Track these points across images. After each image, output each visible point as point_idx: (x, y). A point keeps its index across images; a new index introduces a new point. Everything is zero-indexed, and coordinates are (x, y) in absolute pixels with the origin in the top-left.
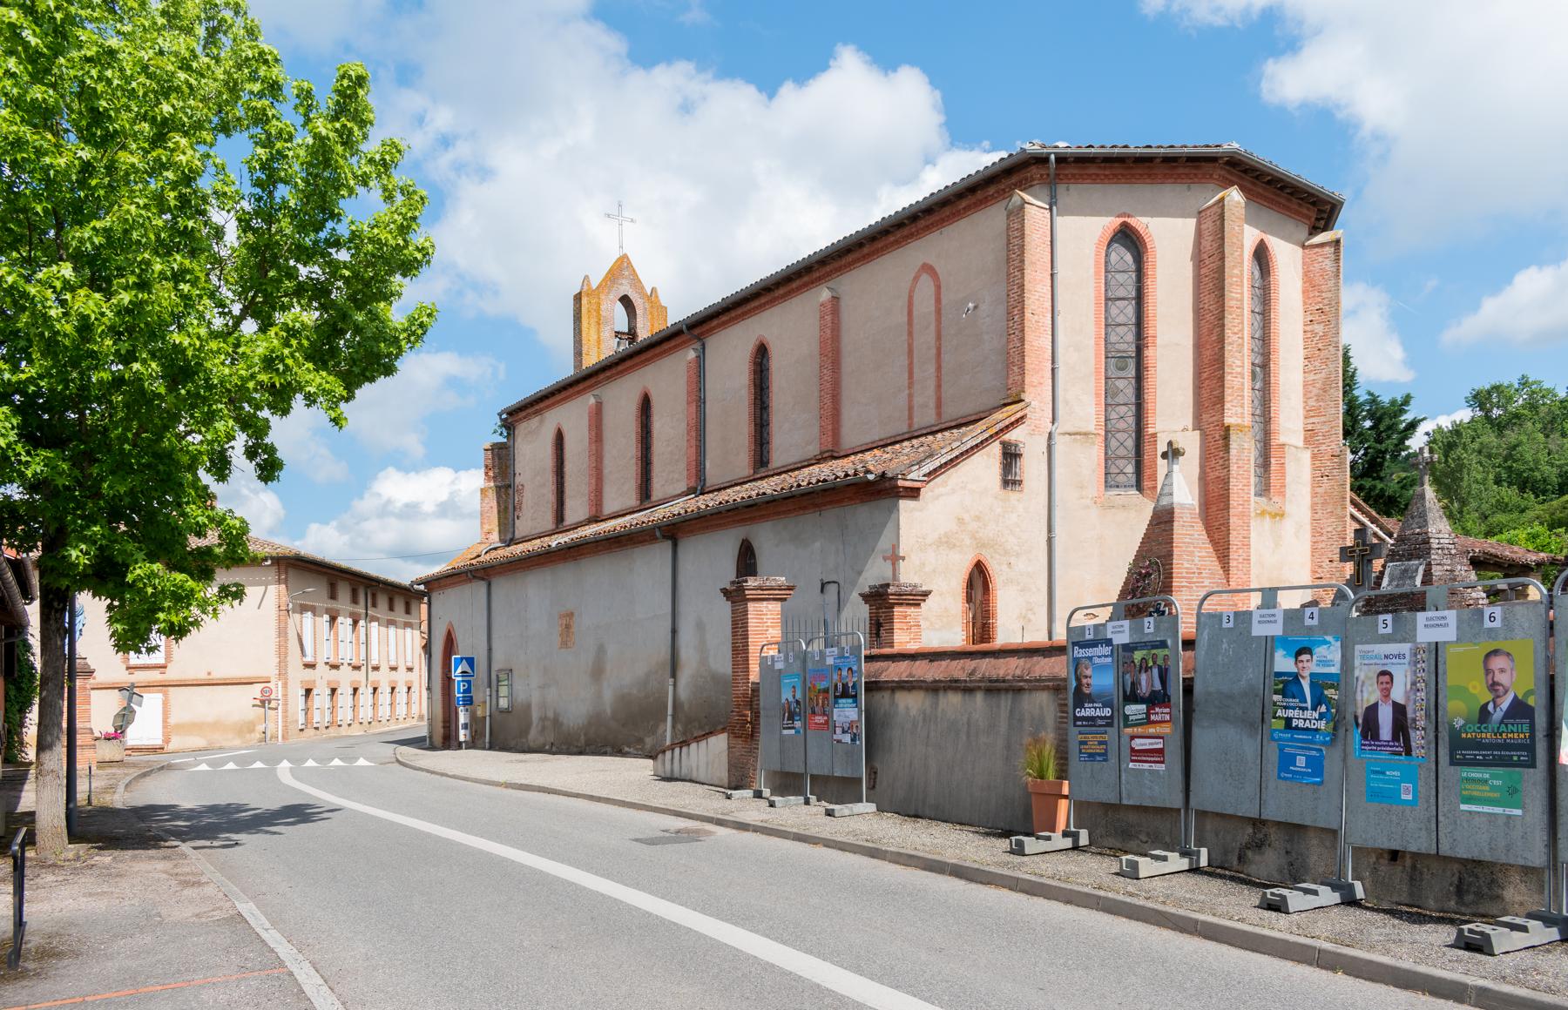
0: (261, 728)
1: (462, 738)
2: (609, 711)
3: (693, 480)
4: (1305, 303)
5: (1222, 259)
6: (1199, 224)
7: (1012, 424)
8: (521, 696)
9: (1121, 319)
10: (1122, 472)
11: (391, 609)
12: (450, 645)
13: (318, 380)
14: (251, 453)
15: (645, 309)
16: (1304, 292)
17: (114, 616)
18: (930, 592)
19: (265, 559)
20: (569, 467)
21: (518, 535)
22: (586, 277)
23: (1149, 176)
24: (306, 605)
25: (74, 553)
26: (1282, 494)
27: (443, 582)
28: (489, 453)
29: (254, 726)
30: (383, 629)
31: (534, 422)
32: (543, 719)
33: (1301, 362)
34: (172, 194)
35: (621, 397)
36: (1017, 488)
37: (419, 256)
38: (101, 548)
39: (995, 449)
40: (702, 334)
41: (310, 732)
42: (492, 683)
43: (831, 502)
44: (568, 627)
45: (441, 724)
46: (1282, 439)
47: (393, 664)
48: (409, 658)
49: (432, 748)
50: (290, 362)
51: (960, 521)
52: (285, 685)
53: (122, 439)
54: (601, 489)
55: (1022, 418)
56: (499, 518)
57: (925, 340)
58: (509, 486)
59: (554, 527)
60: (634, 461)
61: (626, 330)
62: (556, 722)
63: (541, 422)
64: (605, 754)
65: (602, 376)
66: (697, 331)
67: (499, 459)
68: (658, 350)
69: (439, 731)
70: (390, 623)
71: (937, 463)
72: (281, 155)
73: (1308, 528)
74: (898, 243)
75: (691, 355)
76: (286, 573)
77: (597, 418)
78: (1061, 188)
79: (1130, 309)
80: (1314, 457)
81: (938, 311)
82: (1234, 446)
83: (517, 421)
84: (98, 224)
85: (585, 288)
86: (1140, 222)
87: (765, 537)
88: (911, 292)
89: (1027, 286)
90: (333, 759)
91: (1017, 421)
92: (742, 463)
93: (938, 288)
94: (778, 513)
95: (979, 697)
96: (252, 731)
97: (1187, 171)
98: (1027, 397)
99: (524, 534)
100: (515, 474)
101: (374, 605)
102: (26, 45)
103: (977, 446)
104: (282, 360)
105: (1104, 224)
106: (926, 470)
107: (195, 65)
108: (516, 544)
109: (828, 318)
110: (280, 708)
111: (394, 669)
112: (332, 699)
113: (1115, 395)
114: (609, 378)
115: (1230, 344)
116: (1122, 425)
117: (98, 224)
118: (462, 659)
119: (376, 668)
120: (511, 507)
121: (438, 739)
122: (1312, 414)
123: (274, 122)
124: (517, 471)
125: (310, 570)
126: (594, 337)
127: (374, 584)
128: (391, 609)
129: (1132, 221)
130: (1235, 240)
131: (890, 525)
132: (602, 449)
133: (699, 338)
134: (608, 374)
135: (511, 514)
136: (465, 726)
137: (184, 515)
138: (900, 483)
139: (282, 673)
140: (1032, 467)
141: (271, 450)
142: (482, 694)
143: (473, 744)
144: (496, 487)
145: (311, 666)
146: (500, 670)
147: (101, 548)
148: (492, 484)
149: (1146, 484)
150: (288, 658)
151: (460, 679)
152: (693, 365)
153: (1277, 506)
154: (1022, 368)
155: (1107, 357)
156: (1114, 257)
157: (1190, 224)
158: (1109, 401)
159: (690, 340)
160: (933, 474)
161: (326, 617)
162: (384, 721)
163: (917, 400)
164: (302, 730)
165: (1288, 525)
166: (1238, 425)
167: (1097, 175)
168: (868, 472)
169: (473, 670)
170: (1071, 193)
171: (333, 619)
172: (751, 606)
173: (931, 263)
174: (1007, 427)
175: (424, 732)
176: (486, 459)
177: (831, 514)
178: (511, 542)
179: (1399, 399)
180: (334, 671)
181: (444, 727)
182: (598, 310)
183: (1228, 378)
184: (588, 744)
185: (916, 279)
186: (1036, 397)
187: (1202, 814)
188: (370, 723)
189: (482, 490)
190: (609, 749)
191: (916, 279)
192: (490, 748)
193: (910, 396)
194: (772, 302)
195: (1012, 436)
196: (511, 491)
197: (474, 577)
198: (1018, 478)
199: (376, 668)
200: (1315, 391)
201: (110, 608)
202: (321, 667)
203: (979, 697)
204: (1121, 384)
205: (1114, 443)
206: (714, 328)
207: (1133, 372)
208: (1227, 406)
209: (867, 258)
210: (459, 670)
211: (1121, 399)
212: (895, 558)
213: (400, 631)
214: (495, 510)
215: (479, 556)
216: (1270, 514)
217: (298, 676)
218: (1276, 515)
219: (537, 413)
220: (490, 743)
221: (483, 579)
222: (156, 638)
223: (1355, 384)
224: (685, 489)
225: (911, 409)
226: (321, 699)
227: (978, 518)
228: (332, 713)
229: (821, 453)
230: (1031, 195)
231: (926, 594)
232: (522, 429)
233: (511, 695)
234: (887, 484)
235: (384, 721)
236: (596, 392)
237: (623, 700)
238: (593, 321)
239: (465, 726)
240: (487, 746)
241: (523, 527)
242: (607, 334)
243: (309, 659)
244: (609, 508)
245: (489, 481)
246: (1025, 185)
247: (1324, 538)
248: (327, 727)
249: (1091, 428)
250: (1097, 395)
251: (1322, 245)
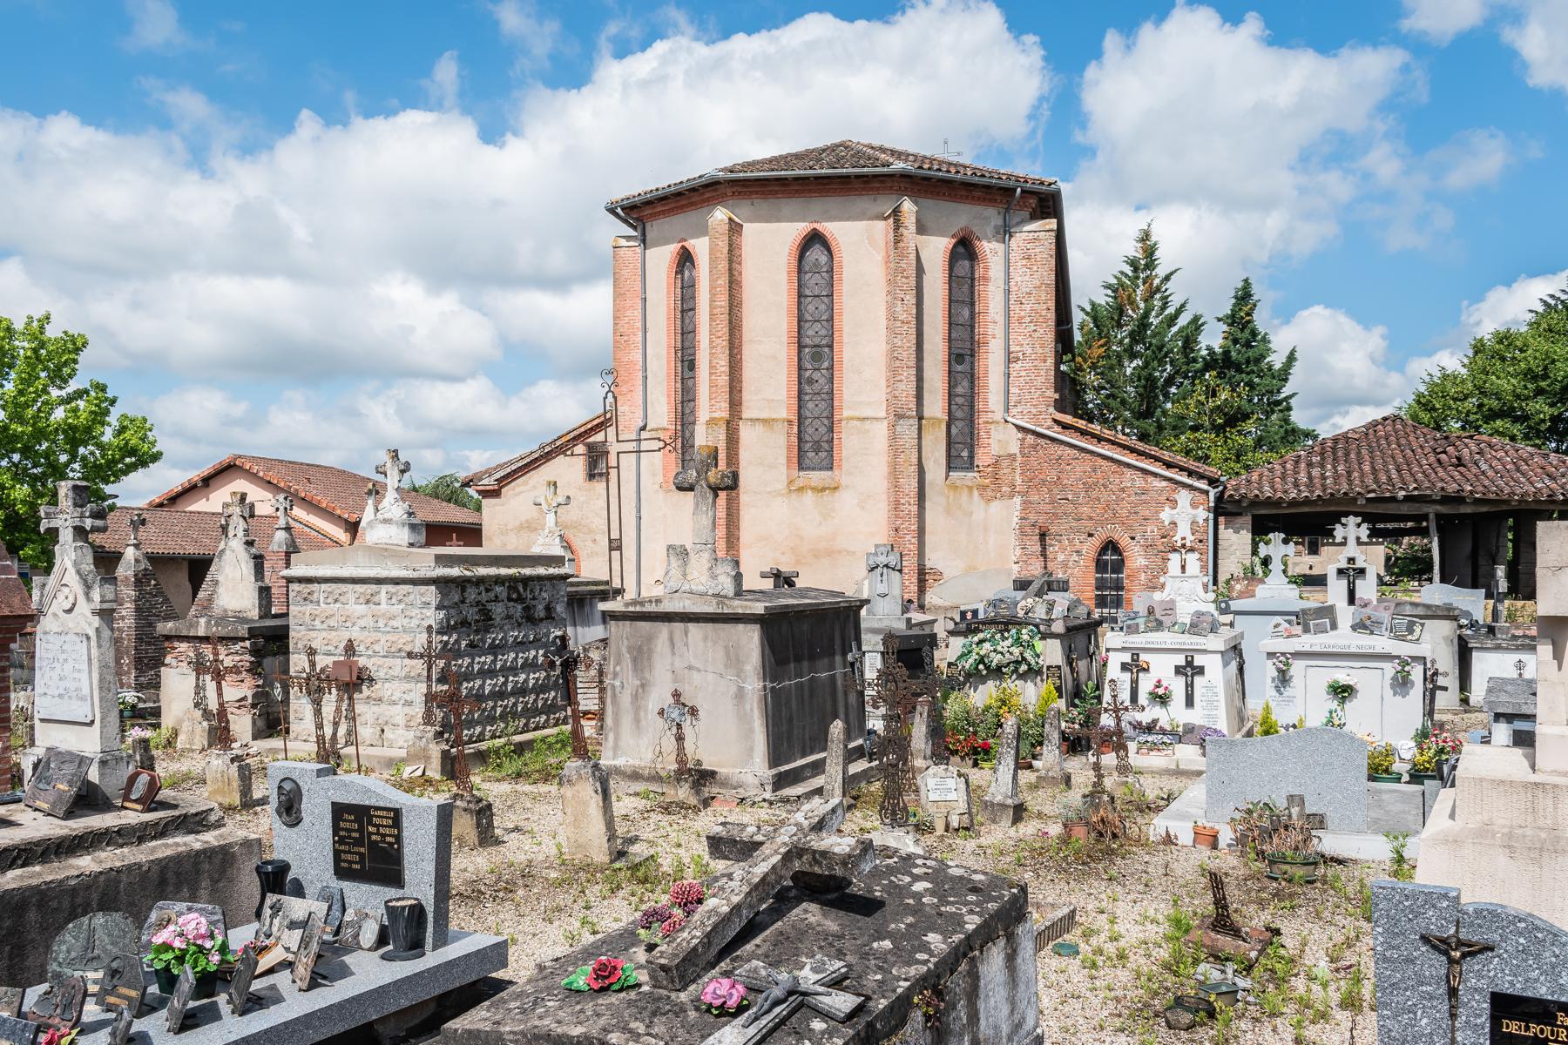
165: (846, 501)
216: (812, 489)
218: (823, 489)
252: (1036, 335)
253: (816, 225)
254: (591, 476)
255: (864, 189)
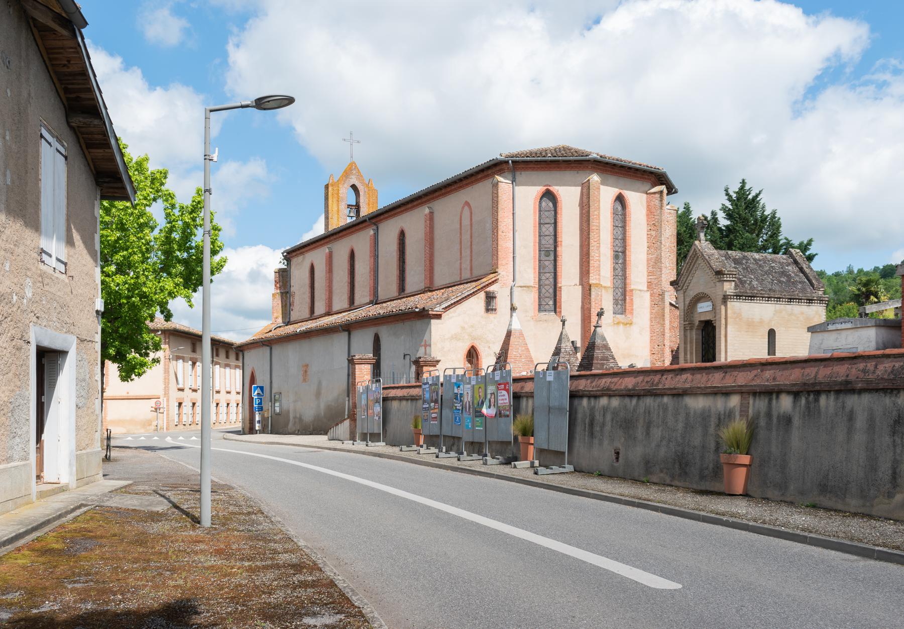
0: (155, 423)
1: (257, 428)
2: (323, 414)
3: (372, 297)
4: (647, 221)
5: (589, 207)
6: (582, 189)
7: (490, 283)
8: (285, 407)
9: (547, 233)
10: (547, 304)
11: (227, 357)
12: (253, 380)
13: (185, 292)
14: (162, 312)
15: (365, 192)
16: (647, 215)
17: (121, 370)
18: (440, 361)
19: (158, 331)
20: (316, 285)
21: (292, 319)
22: (331, 175)
23: (558, 168)
24: (179, 356)
25: (111, 351)
26: (632, 313)
27: (249, 346)
28: (277, 274)
29: (151, 422)
30: (222, 369)
31: (300, 258)
32: (295, 418)
33: (646, 249)
34: (144, 247)
35: (341, 248)
36: (494, 312)
37: (218, 249)
38: (118, 349)
39: (482, 295)
40: (377, 222)
41: (181, 427)
42: (273, 400)
43: (406, 319)
44: (306, 372)
45: (248, 422)
46: (632, 287)
47: (228, 390)
48: (228, 385)
49: (244, 434)
50: (176, 293)
51: (463, 328)
52: (168, 400)
53: (126, 316)
54: (332, 298)
55: (496, 280)
56: (282, 310)
57: (466, 237)
58: (288, 292)
59: (309, 316)
60: (346, 284)
61: (355, 204)
62: (301, 419)
63: (304, 259)
64: (321, 434)
65: (332, 238)
66: (374, 221)
67: (283, 277)
68: (357, 228)
69: (248, 425)
70: (227, 365)
71: (449, 303)
72: (174, 226)
73: (648, 329)
74: (456, 190)
75: (372, 232)
76: (169, 338)
77: (330, 258)
78: (518, 173)
79: (551, 229)
80: (651, 295)
81: (471, 225)
82: (593, 293)
83: (292, 257)
84: (122, 254)
85: (331, 181)
86: (555, 189)
87: (385, 332)
88: (461, 213)
89: (500, 219)
90: (192, 437)
91: (493, 282)
92: (394, 290)
93: (471, 213)
94: (388, 322)
95: (409, 401)
96: (150, 425)
97: (575, 165)
98: (499, 270)
99: (295, 319)
100: (290, 286)
101: (217, 355)
102: (104, 206)
103: (471, 294)
104: (174, 293)
105: (538, 190)
106: (444, 306)
107: (148, 198)
108: (291, 324)
109: (428, 222)
110: (165, 413)
111: (228, 392)
112: (193, 409)
113: (544, 268)
114: (335, 239)
115: (592, 246)
116: (547, 282)
117: (122, 254)
118: (257, 387)
119: (218, 392)
120: (288, 304)
121: (247, 430)
122: (650, 274)
123: (173, 217)
124: (292, 285)
125: (181, 336)
126: (335, 209)
127: (218, 343)
128: (227, 357)
129: (550, 188)
130: (595, 199)
131: (428, 330)
132: (332, 276)
133: (375, 224)
134: (335, 237)
135: (288, 308)
136: (259, 422)
137: (142, 337)
138: (430, 312)
139: (166, 394)
140: (502, 303)
141: (169, 311)
142: (267, 405)
143: (263, 431)
144: (281, 293)
145: (181, 390)
146: (275, 393)
147: (118, 349)
148: (279, 291)
149: (558, 310)
150: (170, 385)
151: (256, 397)
152: (372, 237)
153: (629, 319)
154: (497, 257)
155: (540, 251)
156: (544, 204)
157: (580, 188)
158: (542, 271)
159: (369, 225)
160: (447, 308)
161: (190, 363)
162: (223, 423)
163: (464, 266)
164: (176, 425)
165: (635, 329)
166: (595, 284)
167: (534, 168)
168: (416, 308)
169: (263, 393)
170: (522, 176)
171: (194, 364)
172: (357, 366)
173: (468, 201)
174: (487, 285)
175: (240, 429)
176: (275, 278)
177: (408, 324)
178: (288, 323)
179: (805, 242)
180: (194, 393)
181: (250, 423)
182: (338, 194)
183: (591, 262)
184: (314, 430)
185: (463, 207)
186: (504, 271)
187: (444, 436)
188: (214, 423)
189: (273, 294)
190: (323, 432)
191: (463, 207)
192: (271, 433)
193: (461, 263)
194: (406, 210)
195: (491, 289)
196: (288, 295)
197: (264, 345)
198: (494, 308)
199: (218, 392)
200: (652, 263)
201: (119, 367)
202: (187, 391)
203: (409, 401)
204: (547, 263)
205: (543, 291)
206: (382, 220)
207: (553, 258)
208: (591, 275)
209: (444, 195)
210: (256, 393)
211: (547, 270)
212: (428, 345)
213: (233, 371)
214: (280, 306)
215: (271, 331)
216: (623, 323)
217: (175, 395)
218: (627, 324)
219: (302, 253)
220: (271, 431)
221: (268, 346)
222: (133, 376)
223: (779, 233)
224: (368, 301)
225: (461, 269)
226: (187, 408)
227: (472, 327)
228: (193, 417)
229: (425, 288)
230: (503, 177)
231: (438, 361)
232: (294, 261)
233: (280, 406)
234: (426, 313)
235: (223, 423)
236: (329, 246)
237: (329, 408)
238: (335, 200)
239: (259, 422)
240: (269, 432)
241: (294, 316)
242: (343, 206)
243: (181, 386)
244: (336, 307)
245: (277, 289)
246: (501, 172)
247: (655, 334)
248: (190, 425)
249: (532, 284)
250: (535, 269)
251: (655, 193)
252: (670, 258)
253: (621, 191)
254: (488, 310)
255: (641, 178)
